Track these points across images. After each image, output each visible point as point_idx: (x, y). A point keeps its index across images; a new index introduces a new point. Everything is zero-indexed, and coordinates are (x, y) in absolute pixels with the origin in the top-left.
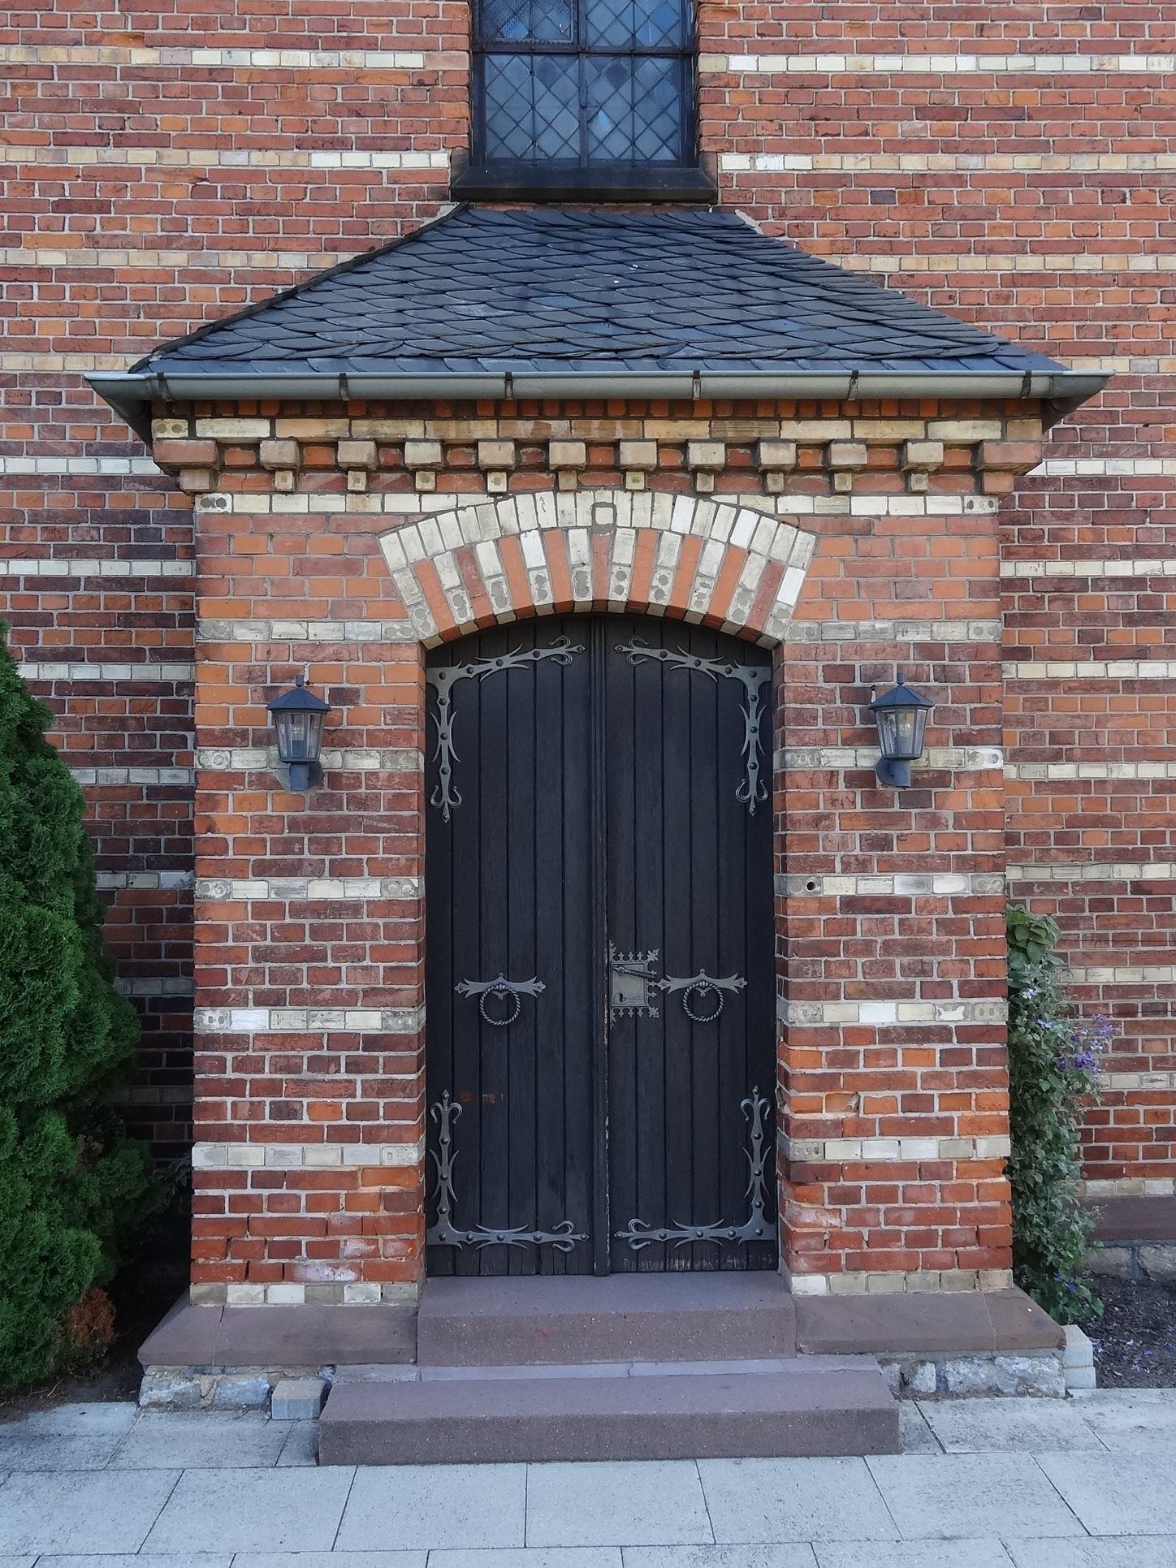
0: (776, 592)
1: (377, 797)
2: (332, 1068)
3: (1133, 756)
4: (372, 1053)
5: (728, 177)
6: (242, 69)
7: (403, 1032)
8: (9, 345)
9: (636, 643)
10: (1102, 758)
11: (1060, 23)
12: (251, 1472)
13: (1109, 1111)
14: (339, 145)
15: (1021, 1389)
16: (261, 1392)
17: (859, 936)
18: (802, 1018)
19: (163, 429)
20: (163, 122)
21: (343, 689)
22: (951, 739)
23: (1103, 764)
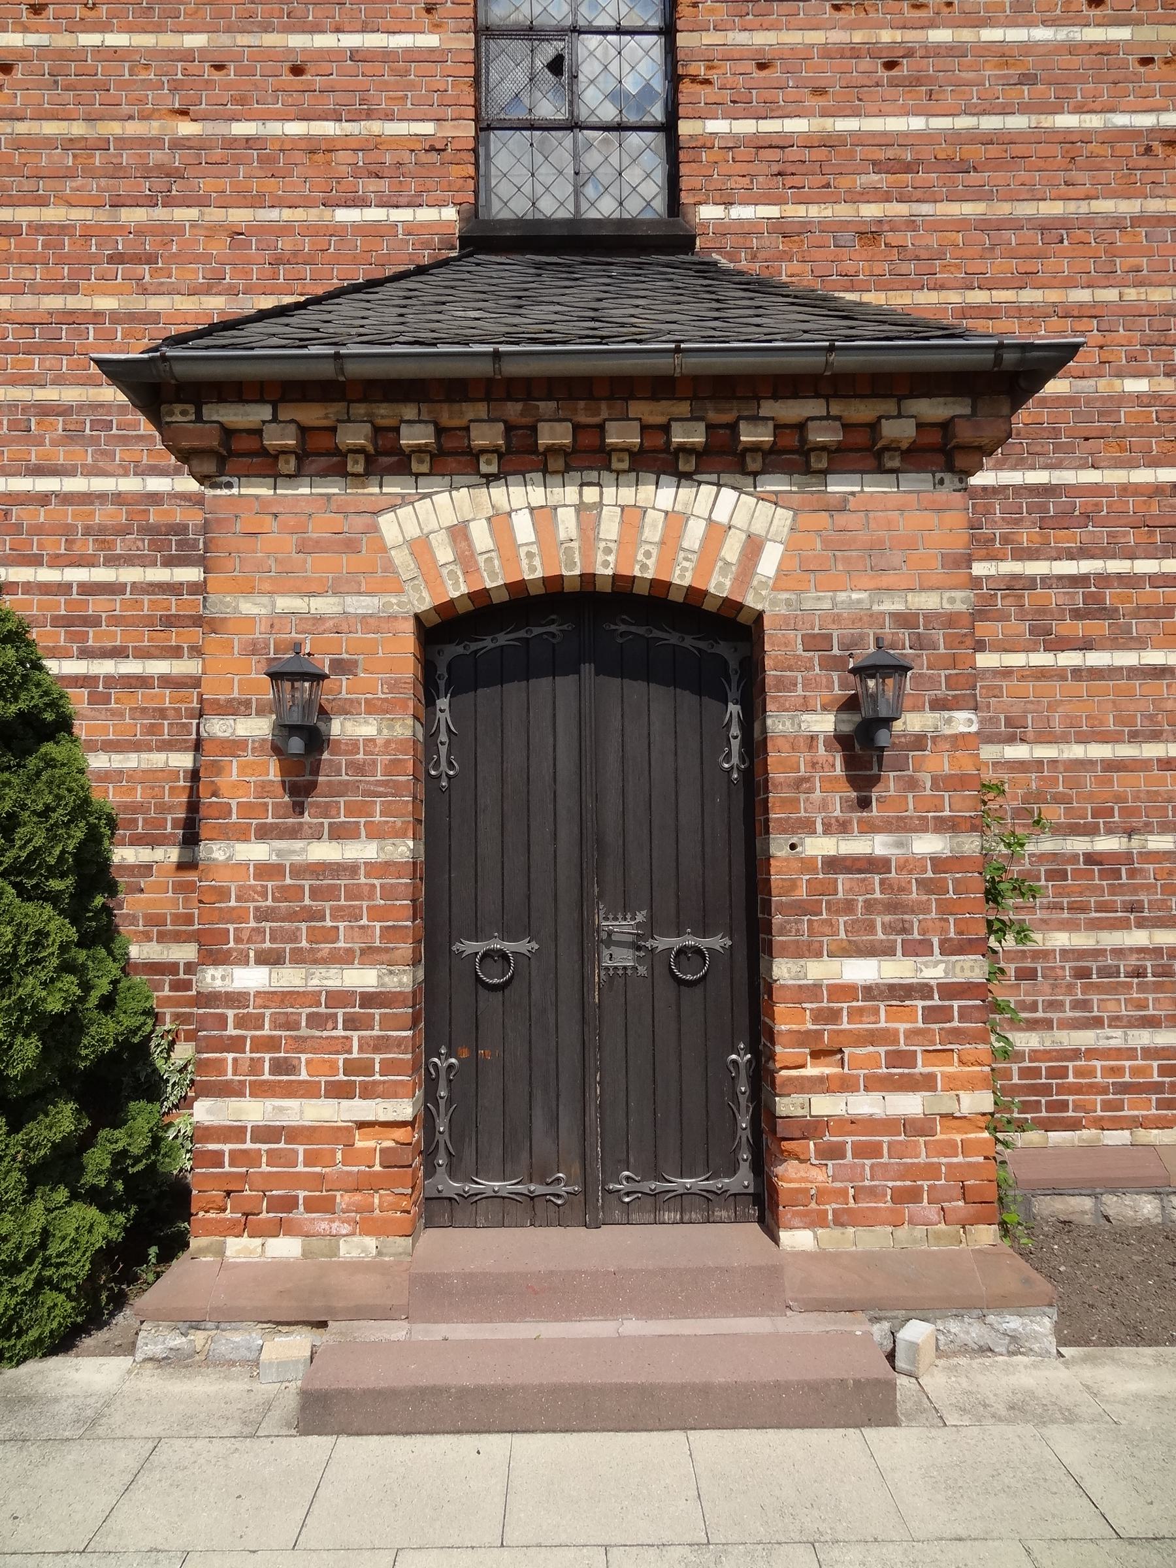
0: (755, 565)
1: (374, 762)
2: (330, 1025)
3: (1083, 739)
4: (369, 1010)
5: (705, 224)
6: (276, 138)
7: (399, 989)
8: (67, 380)
9: (624, 622)
10: (1054, 740)
11: (1000, 87)
12: (228, 1443)
13: (1067, 1067)
14: (363, 203)
15: (1012, 1348)
16: (254, 1348)
17: (840, 895)
18: (786, 975)
19: (172, 414)
20: (205, 186)
21: (342, 659)
22: (927, 704)
23: (1055, 745)
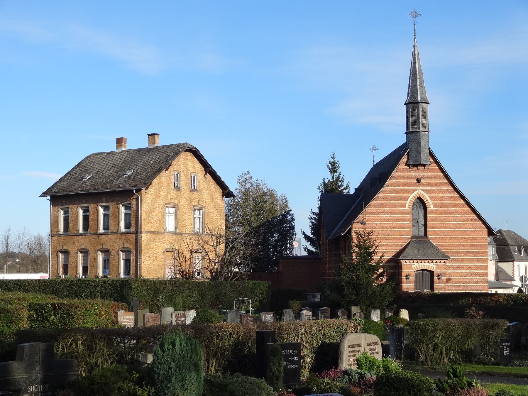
3: (456, 277)
14: (403, 235)
